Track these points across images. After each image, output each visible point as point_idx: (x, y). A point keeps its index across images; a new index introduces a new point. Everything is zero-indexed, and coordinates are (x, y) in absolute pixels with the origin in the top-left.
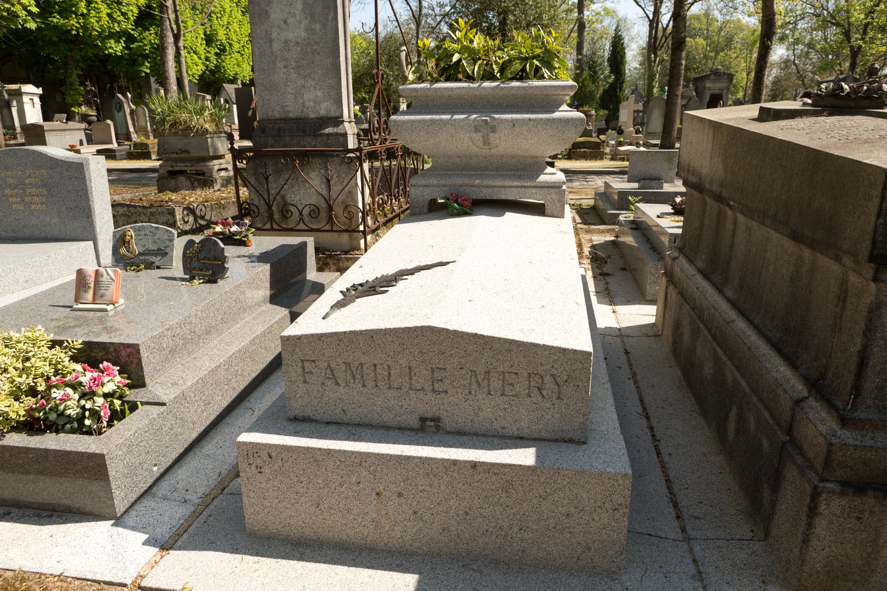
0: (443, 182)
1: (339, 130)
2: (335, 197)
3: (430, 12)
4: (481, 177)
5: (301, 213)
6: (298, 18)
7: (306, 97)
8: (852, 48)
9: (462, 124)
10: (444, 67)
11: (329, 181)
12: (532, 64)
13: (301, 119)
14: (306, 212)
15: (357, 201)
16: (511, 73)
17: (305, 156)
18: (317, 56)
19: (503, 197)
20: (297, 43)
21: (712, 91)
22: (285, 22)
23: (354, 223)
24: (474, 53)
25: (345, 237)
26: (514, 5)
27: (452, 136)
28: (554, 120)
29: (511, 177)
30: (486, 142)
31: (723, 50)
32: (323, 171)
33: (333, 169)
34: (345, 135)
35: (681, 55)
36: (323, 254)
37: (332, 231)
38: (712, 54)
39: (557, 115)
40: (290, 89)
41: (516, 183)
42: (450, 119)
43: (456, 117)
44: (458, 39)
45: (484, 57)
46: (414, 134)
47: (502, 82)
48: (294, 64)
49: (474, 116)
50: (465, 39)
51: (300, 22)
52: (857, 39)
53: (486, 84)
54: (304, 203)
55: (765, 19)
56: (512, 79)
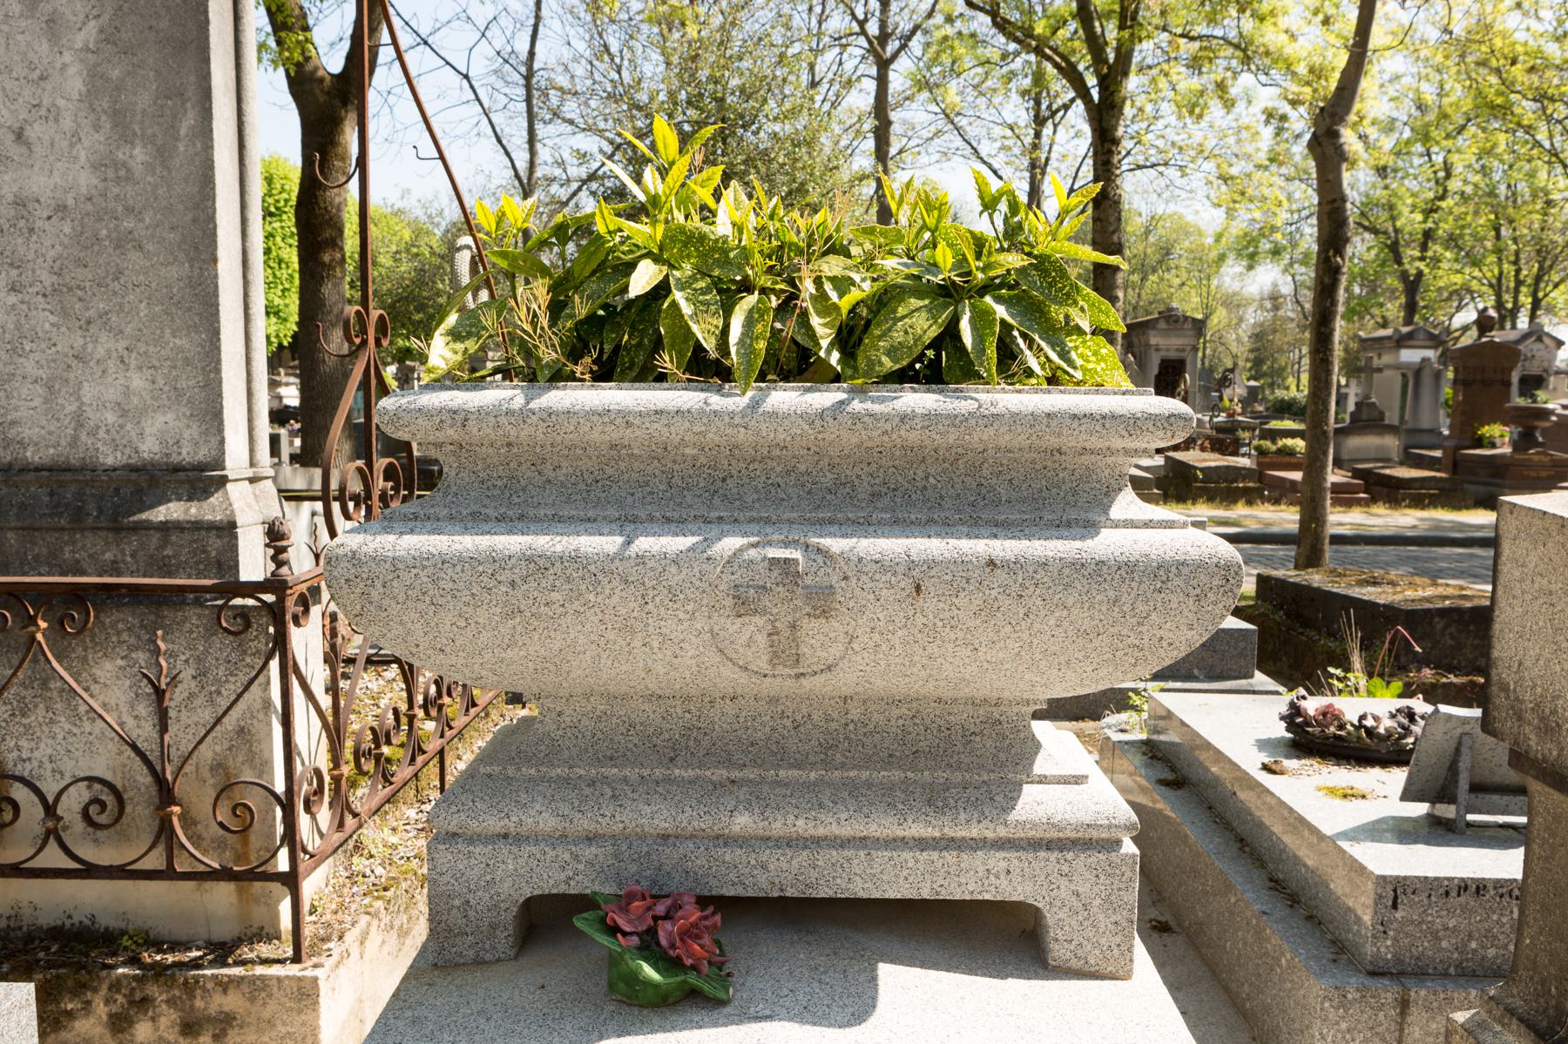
0: (584, 823)
1: (208, 510)
2: (186, 747)
3: (558, 172)
4: (757, 797)
5: (50, 810)
6: (67, 123)
7: (88, 393)
8: (1404, 276)
9: (674, 577)
10: (592, 318)
11: (159, 694)
12: (982, 319)
13: (68, 469)
14: (71, 806)
15: (267, 764)
16: (892, 352)
17: (74, 606)
18: (134, 256)
19: (862, 889)
20: (62, 208)
21: (1163, 353)
22: (19, 136)
23: (255, 840)
24: (725, 262)
25: (222, 895)
26: (745, 162)
27: (627, 628)
28: (1097, 571)
29: (891, 798)
30: (785, 651)
31: (1154, 271)
32: (141, 657)
33: (181, 649)
34: (228, 529)
35: (1114, 280)
36: (134, 961)
37: (168, 874)
38: (1136, 278)
39: (1108, 543)
40: (29, 366)
41: (916, 830)
42: (620, 556)
43: (646, 544)
44: (655, 200)
45: (766, 281)
46: (448, 619)
47: (860, 391)
48: (48, 280)
49: (730, 544)
50: (683, 202)
51: (76, 138)
52: (1413, 259)
53: (786, 398)
54: (70, 768)
55: (1327, 208)
56: (903, 377)
